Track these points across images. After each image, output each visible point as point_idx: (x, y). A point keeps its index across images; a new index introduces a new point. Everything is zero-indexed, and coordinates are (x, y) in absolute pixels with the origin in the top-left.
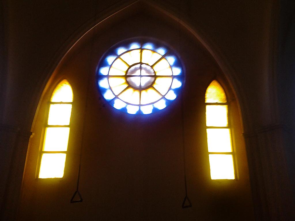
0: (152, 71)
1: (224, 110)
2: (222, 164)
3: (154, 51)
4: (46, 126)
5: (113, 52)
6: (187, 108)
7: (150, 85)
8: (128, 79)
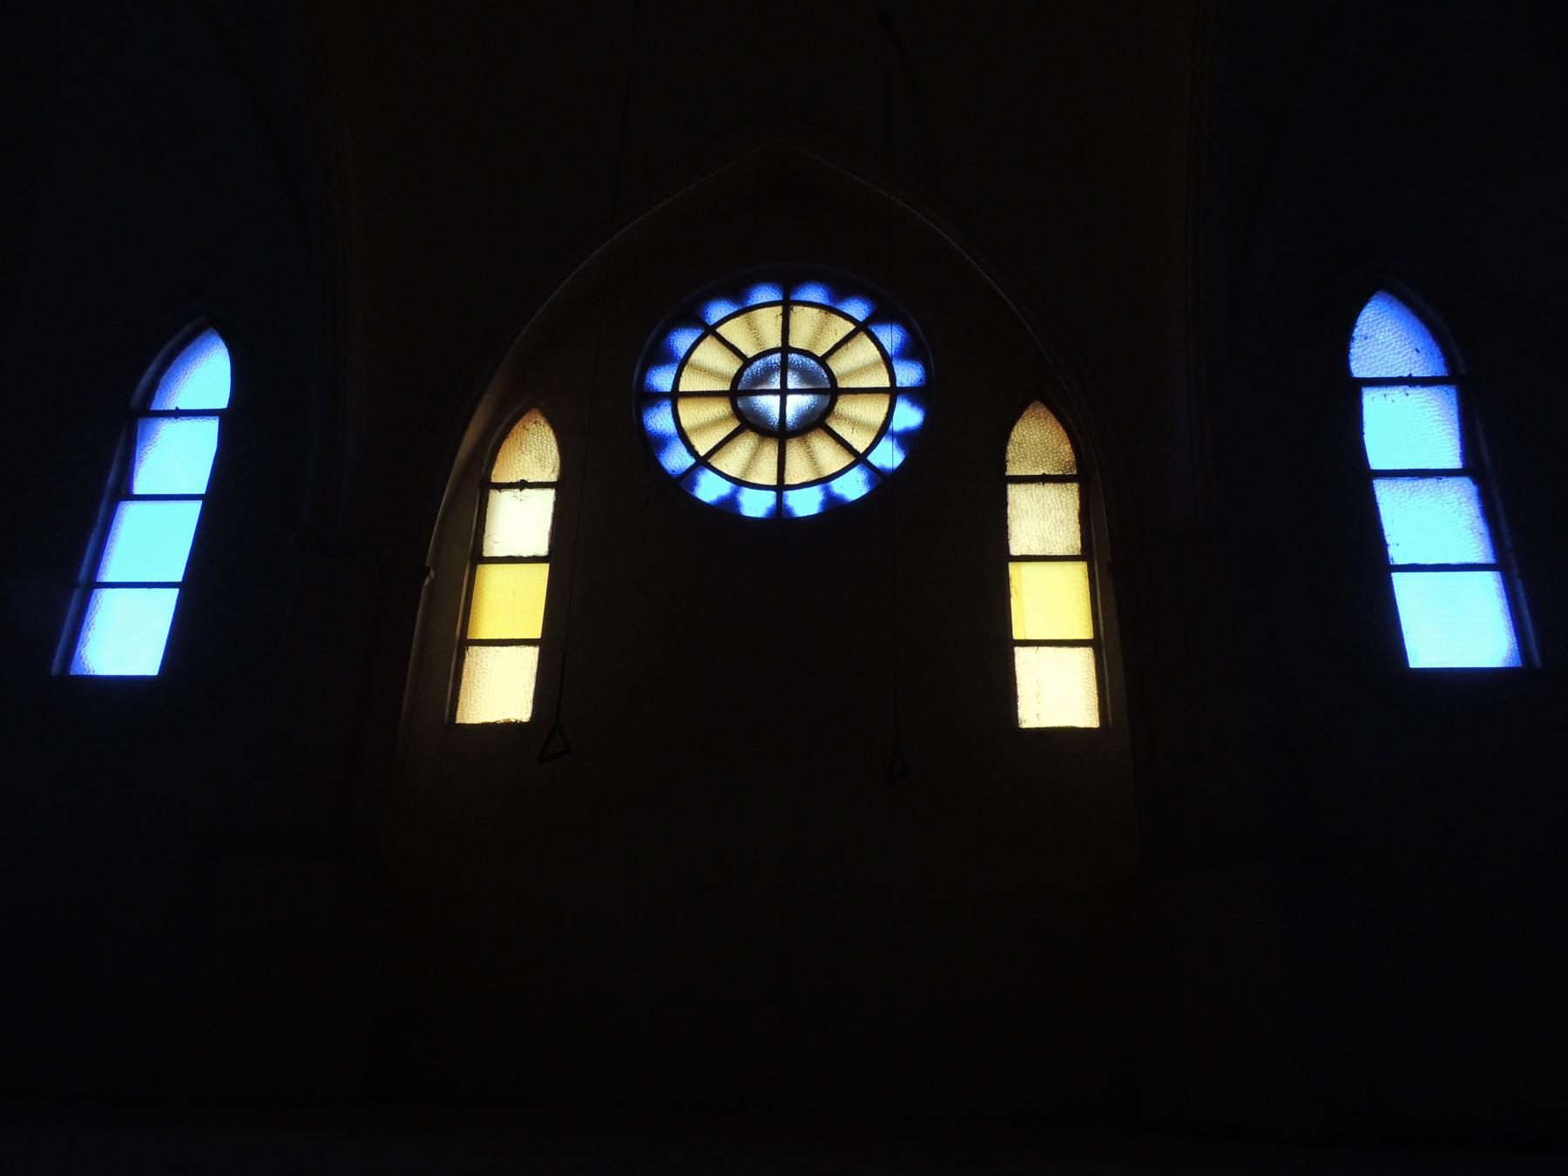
7: (816, 422)
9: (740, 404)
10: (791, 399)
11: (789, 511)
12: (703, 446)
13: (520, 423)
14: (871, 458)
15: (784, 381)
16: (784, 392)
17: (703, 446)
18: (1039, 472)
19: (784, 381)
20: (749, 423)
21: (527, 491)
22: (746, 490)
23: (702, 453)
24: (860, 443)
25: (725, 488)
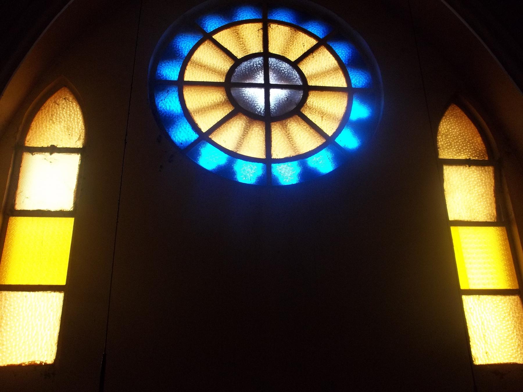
9: (233, 92)
10: (261, 92)
11: (233, 173)
12: (205, 125)
13: (52, 98)
14: (338, 140)
15: (267, 78)
16: (267, 86)
17: (205, 125)
18: (463, 157)
19: (267, 78)
20: (240, 109)
21: (56, 155)
22: (239, 162)
23: (204, 129)
24: (329, 129)
25: (222, 159)
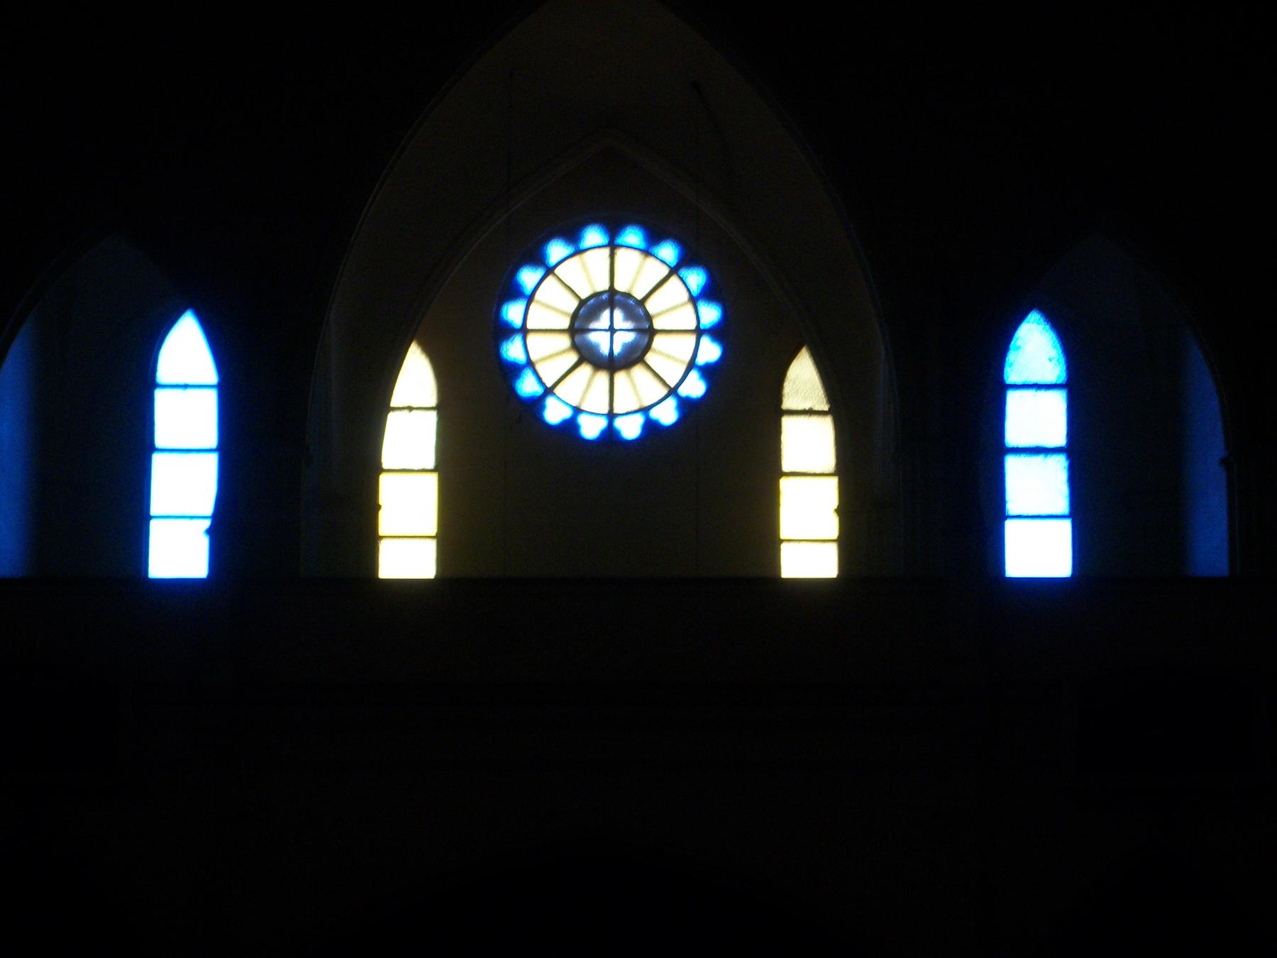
0: (641, 311)
1: (825, 428)
2: (809, 535)
3: (647, 253)
4: (381, 470)
5: (536, 258)
6: (734, 420)
8: (577, 339)
